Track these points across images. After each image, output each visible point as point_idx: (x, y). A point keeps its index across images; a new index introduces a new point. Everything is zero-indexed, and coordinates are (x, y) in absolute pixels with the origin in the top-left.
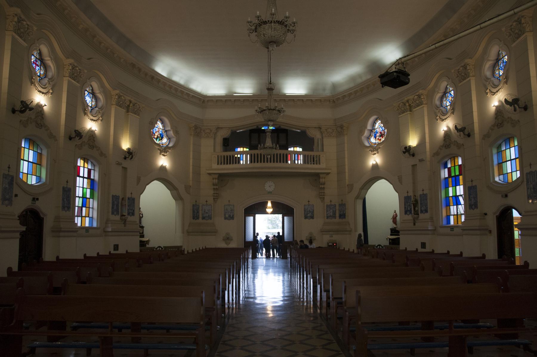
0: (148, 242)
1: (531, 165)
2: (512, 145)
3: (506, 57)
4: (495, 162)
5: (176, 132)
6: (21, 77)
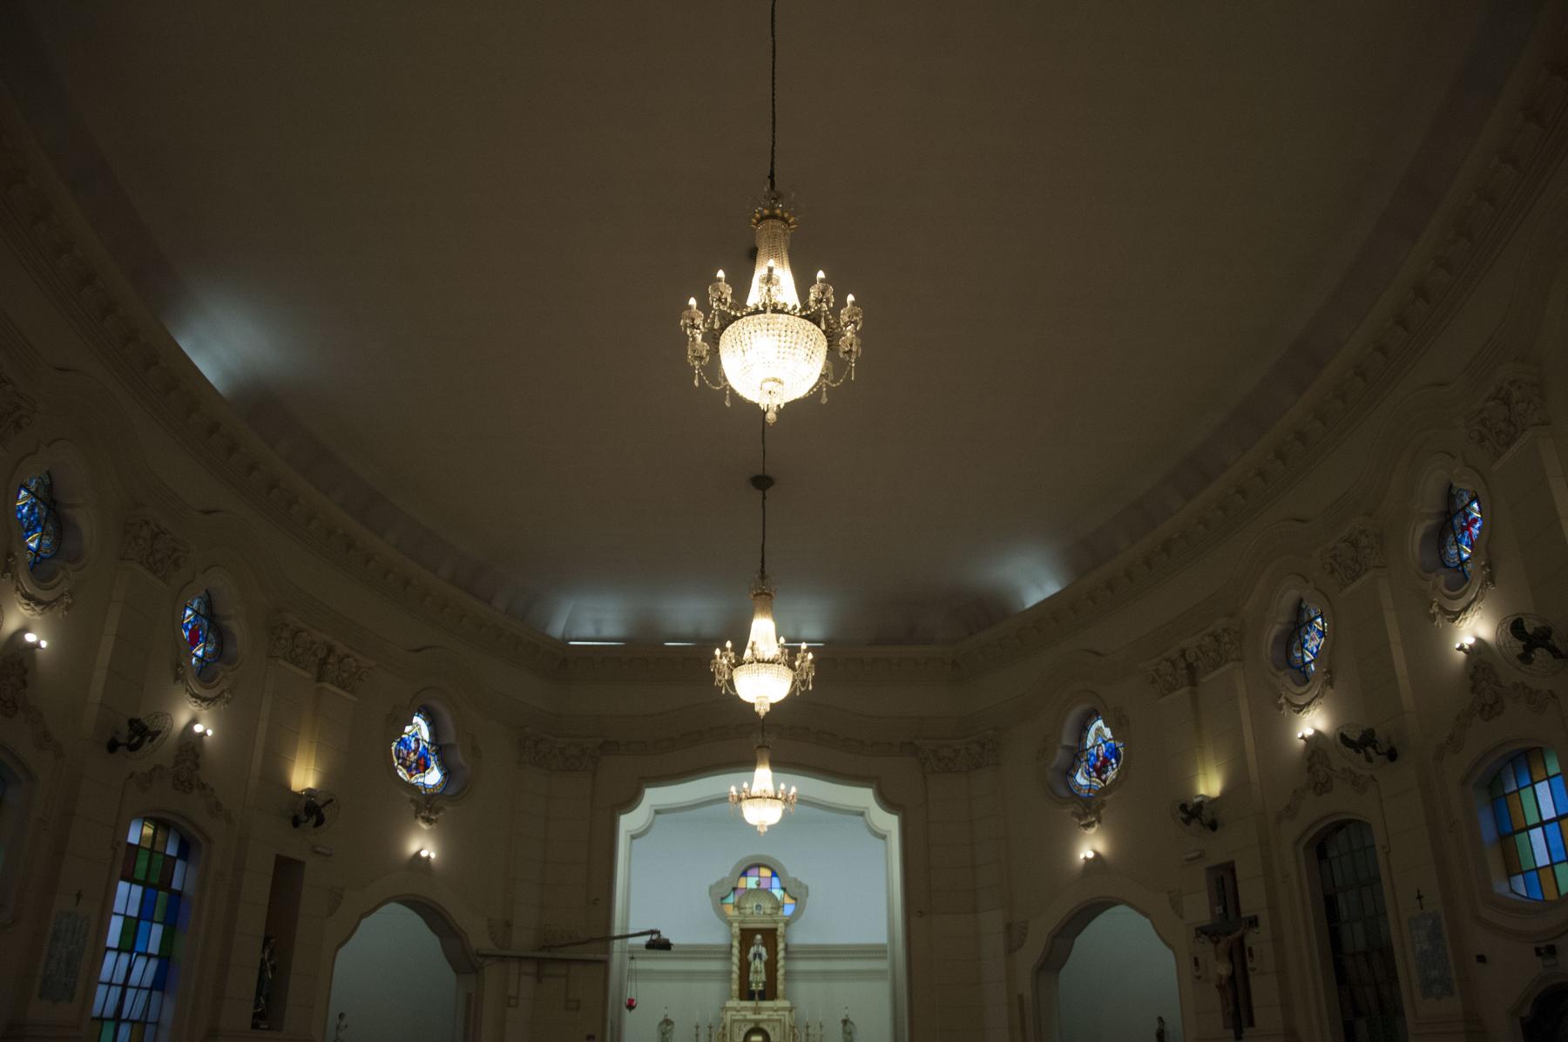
1: (1420, 897)
3: (1475, 505)
4: (1488, 831)
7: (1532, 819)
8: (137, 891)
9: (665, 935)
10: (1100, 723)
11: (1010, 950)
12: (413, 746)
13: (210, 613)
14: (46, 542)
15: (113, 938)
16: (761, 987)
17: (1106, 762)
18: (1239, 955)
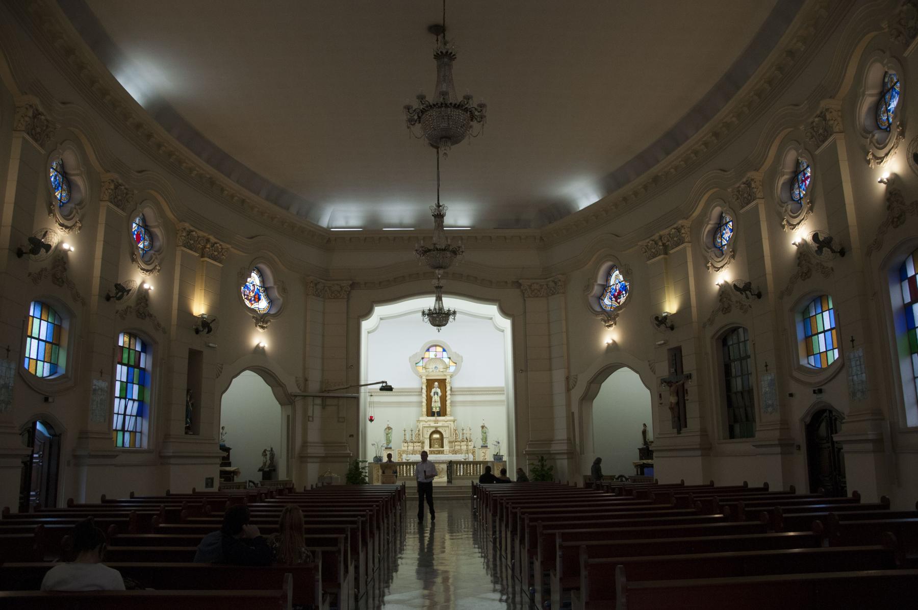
0: (235, 473)
1: (853, 341)
2: (825, 308)
3: (809, 169)
4: (800, 335)
5: (283, 290)
6: (32, 204)
7: (820, 329)
8: (125, 368)
9: (389, 384)
10: (617, 272)
11: (568, 390)
12: (252, 288)
13: (145, 225)
14: (64, 194)
15: (117, 394)
16: (438, 410)
17: (620, 293)
18: (681, 393)
